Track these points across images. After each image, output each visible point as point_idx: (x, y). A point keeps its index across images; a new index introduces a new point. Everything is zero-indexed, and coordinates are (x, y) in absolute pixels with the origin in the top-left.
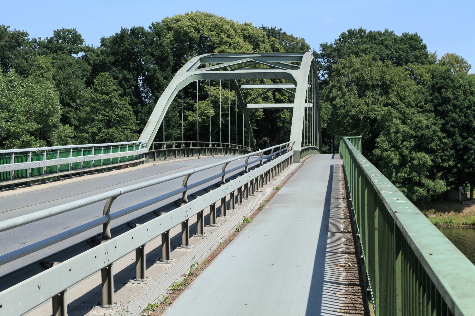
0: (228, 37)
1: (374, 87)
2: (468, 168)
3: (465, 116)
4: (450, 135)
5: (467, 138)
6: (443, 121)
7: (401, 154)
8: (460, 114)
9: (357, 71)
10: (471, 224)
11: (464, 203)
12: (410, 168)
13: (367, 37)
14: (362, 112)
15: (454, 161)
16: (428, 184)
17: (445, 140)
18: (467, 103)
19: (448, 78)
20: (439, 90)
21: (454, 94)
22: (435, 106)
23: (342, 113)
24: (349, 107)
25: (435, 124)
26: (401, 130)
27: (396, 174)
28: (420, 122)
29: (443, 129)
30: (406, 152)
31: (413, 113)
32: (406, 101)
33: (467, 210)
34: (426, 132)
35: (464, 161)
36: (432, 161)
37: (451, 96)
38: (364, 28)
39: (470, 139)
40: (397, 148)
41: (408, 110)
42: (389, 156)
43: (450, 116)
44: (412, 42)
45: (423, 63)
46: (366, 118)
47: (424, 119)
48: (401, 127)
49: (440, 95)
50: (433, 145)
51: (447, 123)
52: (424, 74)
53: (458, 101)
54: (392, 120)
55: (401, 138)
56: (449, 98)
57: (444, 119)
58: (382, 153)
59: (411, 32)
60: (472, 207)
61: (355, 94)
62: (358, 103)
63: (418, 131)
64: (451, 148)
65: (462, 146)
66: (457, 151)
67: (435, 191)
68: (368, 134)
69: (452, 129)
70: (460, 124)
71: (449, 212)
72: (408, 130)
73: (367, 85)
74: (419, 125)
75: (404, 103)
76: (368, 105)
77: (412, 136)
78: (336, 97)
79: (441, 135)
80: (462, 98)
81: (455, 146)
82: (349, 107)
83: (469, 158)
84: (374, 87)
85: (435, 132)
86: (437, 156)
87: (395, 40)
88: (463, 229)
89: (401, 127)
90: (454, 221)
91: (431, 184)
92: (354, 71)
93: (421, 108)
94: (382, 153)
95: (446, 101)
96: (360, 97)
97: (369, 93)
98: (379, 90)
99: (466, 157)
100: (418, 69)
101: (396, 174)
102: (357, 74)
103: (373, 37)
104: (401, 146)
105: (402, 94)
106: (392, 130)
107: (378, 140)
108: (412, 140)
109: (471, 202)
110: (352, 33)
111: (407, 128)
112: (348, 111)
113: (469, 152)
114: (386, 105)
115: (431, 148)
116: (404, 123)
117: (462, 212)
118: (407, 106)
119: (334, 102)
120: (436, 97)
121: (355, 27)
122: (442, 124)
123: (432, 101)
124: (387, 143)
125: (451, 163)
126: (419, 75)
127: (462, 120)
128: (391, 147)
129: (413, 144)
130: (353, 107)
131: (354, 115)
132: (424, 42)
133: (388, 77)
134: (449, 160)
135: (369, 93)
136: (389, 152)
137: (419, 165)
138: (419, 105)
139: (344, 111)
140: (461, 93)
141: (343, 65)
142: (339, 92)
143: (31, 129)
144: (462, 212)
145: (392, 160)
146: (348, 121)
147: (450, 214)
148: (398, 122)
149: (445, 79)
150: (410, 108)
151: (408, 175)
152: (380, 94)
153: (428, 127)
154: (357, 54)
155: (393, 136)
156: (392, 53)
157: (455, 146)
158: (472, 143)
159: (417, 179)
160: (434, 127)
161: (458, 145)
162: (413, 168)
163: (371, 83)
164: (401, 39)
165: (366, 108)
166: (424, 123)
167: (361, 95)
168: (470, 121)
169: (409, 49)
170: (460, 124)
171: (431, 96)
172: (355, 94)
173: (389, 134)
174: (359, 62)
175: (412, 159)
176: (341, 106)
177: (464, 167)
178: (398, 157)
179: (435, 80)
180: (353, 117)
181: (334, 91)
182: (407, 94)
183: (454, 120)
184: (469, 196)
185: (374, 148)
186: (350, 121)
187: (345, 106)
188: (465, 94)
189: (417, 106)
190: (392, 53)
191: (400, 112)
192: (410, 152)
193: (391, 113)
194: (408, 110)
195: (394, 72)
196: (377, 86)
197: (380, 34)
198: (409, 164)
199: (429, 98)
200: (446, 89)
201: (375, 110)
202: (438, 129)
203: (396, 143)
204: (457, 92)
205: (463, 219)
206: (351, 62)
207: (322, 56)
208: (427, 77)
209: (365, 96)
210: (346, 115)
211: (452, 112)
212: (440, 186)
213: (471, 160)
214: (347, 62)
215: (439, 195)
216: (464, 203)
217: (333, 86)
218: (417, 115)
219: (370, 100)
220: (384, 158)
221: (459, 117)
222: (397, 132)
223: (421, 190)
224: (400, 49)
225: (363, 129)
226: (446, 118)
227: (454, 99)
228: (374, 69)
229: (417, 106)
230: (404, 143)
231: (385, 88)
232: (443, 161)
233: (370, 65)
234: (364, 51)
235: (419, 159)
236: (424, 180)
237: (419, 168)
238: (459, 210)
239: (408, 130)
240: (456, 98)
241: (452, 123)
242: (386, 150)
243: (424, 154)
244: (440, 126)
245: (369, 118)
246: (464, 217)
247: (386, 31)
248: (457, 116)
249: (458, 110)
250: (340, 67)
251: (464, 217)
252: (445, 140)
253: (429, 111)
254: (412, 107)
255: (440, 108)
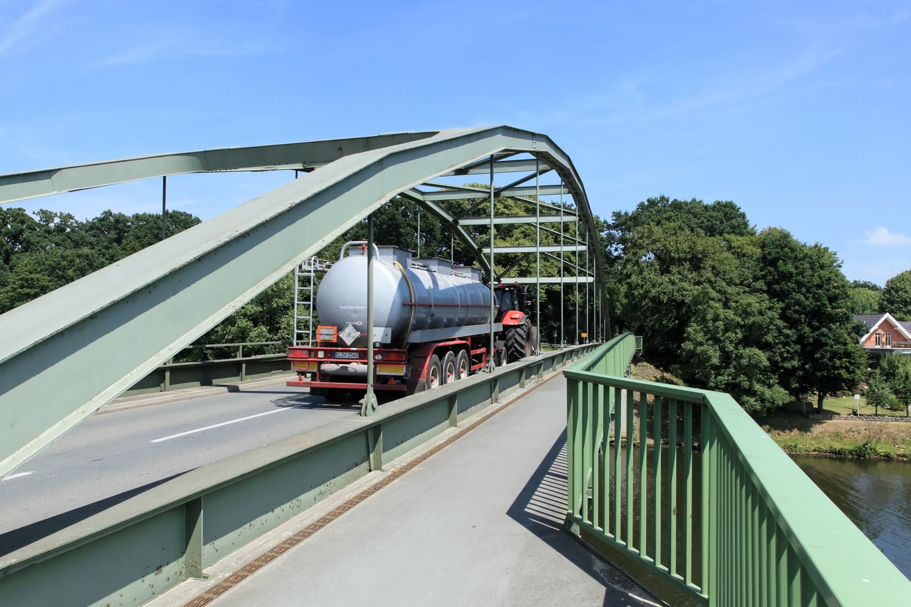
0: (506, 207)
1: (680, 261)
2: (820, 371)
3: (814, 298)
4: (793, 324)
5: (818, 329)
6: (781, 305)
7: (722, 349)
8: (808, 295)
9: (659, 241)
10: (826, 451)
11: (811, 417)
12: (735, 368)
13: (670, 206)
14: (665, 293)
15: (799, 360)
16: (763, 393)
17: (786, 331)
18: (816, 281)
19: (786, 246)
20: (773, 263)
21: (796, 268)
22: (769, 284)
23: (640, 294)
24: (648, 286)
25: (770, 309)
26: (722, 316)
27: (716, 377)
28: (749, 305)
29: (783, 316)
30: (730, 347)
31: (738, 294)
32: (727, 277)
33: (817, 429)
34: (758, 319)
35: (815, 361)
36: (768, 359)
37: (793, 270)
38: (666, 196)
39: (824, 330)
40: (716, 341)
41: (730, 290)
42: (704, 352)
43: (792, 298)
44: (727, 210)
45: (742, 235)
46: (671, 300)
47: (754, 301)
48: (722, 312)
49: (776, 269)
50: (769, 338)
51: (788, 307)
52: (746, 246)
53: (803, 277)
54: (707, 302)
55: (722, 327)
56: (791, 274)
57: (783, 302)
58: (695, 348)
59: (724, 199)
60: (824, 425)
61: (656, 270)
62: (660, 281)
63: (746, 318)
64: (795, 342)
65: (811, 340)
66: (804, 346)
67: (773, 403)
68: (674, 321)
69: (796, 316)
70: (808, 309)
71: (791, 430)
72: (732, 316)
73: (672, 259)
74: (749, 310)
75: (724, 280)
76: (673, 283)
77: (738, 325)
78: (631, 274)
79: (781, 323)
80: (809, 272)
81: (800, 340)
82: (648, 286)
83: (822, 357)
84: (680, 261)
85: (772, 319)
86: (774, 353)
87: (706, 208)
88: (815, 457)
89: (722, 312)
90: (800, 446)
91: (768, 393)
92: (654, 242)
93: (749, 286)
94: (695, 348)
95: (786, 277)
96: (662, 274)
97: (674, 269)
98: (687, 265)
99: (818, 355)
100: (737, 241)
101: (716, 377)
102: (659, 245)
103: (677, 206)
104: (722, 339)
105: (721, 268)
106: (709, 317)
107: (690, 329)
108: (738, 331)
109: (820, 416)
110: (652, 203)
111: (730, 314)
112: (647, 292)
113: (822, 348)
114: (698, 283)
115: (767, 341)
116: (726, 306)
117: (810, 431)
118: (728, 284)
119: (628, 280)
120: (770, 272)
121: (655, 195)
122: (781, 309)
123: (764, 277)
124: (702, 334)
125: (795, 363)
126: (739, 247)
127: (809, 303)
128: (708, 340)
129: (740, 335)
130: (654, 286)
131: (654, 297)
132: (741, 211)
133: (700, 248)
134: (792, 358)
135: (674, 269)
136: (705, 347)
137: (750, 365)
138: (745, 282)
139: (641, 292)
140: (808, 265)
141: (640, 235)
142: (636, 268)
143: (249, 313)
144: (810, 431)
145: (709, 358)
146: (647, 304)
147: (793, 434)
148: (717, 305)
149: (782, 249)
150: (734, 287)
151: (733, 379)
152: (689, 269)
153: (761, 313)
154: (658, 223)
155: (710, 324)
156: (702, 222)
157: (800, 340)
158: (826, 336)
159: (746, 384)
160: (770, 313)
161: (805, 338)
162: (740, 369)
163: (677, 256)
164: (714, 208)
165: (670, 287)
166: (756, 307)
167: (665, 271)
168: (824, 305)
169: (725, 219)
170: (808, 309)
171: (761, 271)
172: (656, 270)
173: (704, 320)
174: (661, 231)
175: (739, 357)
176: (638, 285)
177: (814, 369)
178: (718, 353)
179: (767, 250)
180: (653, 299)
181: (629, 266)
182: (728, 267)
183: (798, 303)
184: (816, 406)
185: (683, 340)
186: (650, 304)
187: (642, 286)
188: (812, 268)
189: (741, 284)
190: (702, 222)
191: (719, 291)
192: (736, 348)
193: (708, 293)
194: (730, 290)
195: (704, 242)
196: (685, 259)
197: (686, 204)
198: (734, 363)
199: (759, 273)
200: (784, 261)
201: (684, 290)
202: (777, 316)
203: (715, 333)
204: (802, 264)
205: (813, 442)
206: (651, 232)
207: (615, 227)
208: (749, 249)
209: (668, 272)
210: (644, 296)
211: (794, 291)
212: (780, 395)
213: (825, 360)
214: (646, 230)
215: (778, 407)
216: (811, 417)
217: (628, 261)
218: (743, 296)
219: (676, 278)
220: (698, 355)
221: (807, 298)
222: (716, 319)
223: (752, 400)
224: (712, 217)
225: (666, 315)
226: (787, 301)
227: (798, 274)
228: (681, 239)
229: (741, 284)
230: (727, 335)
231: (696, 263)
232: (784, 359)
233: (676, 234)
234: (668, 219)
235: (750, 357)
236: (757, 387)
237: (750, 370)
238: (805, 428)
239: (732, 316)
240: (801, 273)
241: (797, 307)
242: (701, 344)
243: (756, 350)
244: (780, 311)
245: (674, 301)
246: (814, 439)
247: (694, 200)
248: (803, 298)
249: (804, 290)
250: (637, 236)
251: (814, 439)
252: (786, 331)
253: (760, 291)
254: (736, 285)
255: (776, 287)
